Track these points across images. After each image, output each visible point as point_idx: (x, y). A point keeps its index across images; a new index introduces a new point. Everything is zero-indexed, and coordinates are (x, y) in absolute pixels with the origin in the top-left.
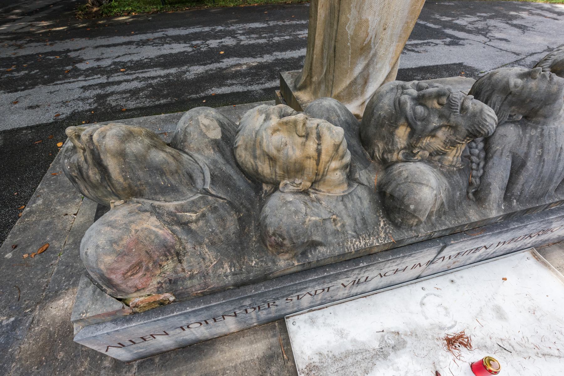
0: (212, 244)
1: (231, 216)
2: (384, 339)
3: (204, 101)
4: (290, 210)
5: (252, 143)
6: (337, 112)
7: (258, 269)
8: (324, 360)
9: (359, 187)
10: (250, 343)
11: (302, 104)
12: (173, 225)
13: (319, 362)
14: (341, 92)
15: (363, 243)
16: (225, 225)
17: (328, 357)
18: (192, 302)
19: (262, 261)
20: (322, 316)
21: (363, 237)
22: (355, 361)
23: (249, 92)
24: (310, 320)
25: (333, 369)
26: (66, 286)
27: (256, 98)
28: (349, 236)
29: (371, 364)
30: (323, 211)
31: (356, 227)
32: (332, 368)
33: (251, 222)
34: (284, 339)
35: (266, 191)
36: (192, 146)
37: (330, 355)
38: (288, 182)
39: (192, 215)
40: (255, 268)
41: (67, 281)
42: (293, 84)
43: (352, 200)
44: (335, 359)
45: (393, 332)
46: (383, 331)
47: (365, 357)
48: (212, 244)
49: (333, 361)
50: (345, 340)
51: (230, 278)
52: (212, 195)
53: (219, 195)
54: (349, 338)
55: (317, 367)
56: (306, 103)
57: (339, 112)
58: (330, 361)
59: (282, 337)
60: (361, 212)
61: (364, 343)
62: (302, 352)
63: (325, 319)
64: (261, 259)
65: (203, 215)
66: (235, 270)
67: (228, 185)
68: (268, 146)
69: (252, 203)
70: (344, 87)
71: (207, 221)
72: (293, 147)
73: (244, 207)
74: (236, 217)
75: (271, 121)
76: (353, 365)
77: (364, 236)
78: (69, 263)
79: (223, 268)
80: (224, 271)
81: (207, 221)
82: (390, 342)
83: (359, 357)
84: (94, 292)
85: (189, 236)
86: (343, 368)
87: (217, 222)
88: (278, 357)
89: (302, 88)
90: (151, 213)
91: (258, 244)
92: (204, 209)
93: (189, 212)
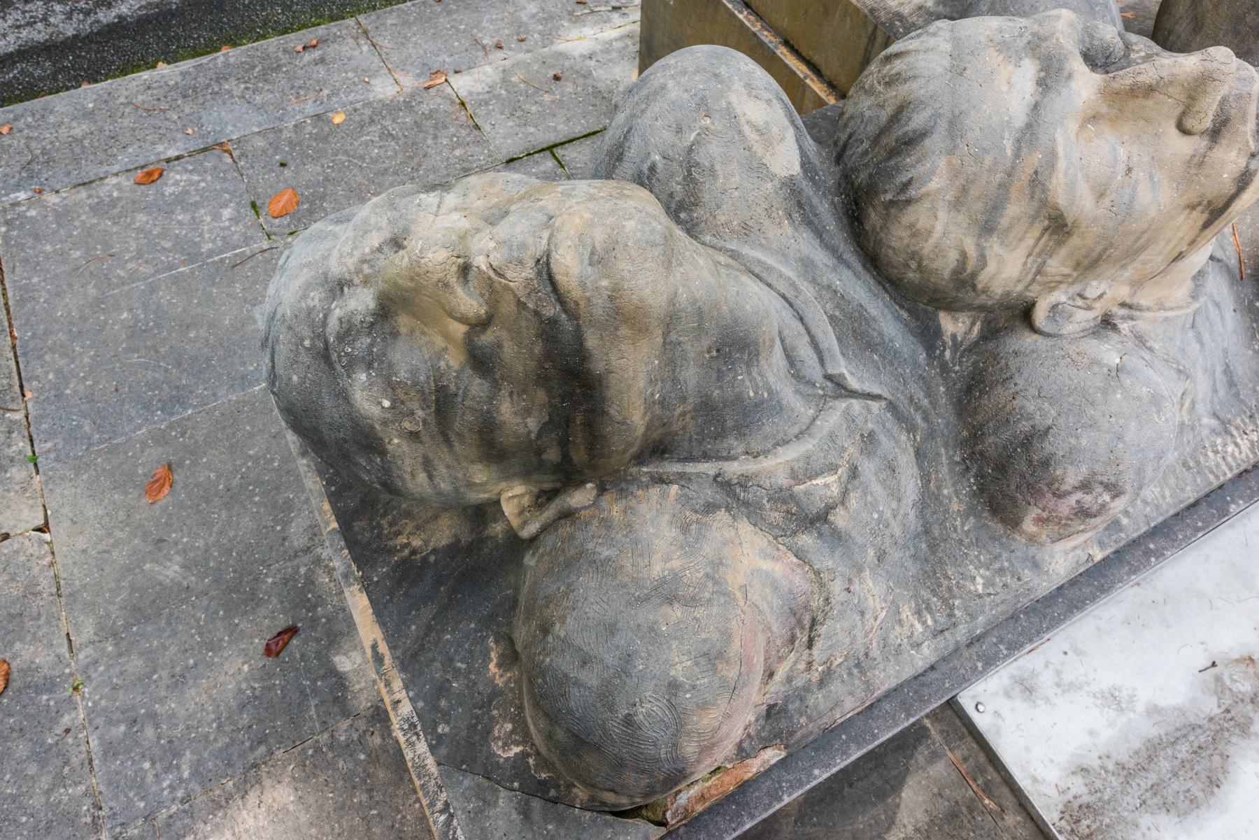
2: (1223, 685)
4: (1139, 399)
5: (999, 177)
7: (998, 599)
8: (1098, 784)
10: (878, 797)
12: (794, 533)
13: (1090, 793)
15: (1245, 445)
17: (1106, 771)
18: (816, 750)
19: (1001, 571)
20: (1046, 666)
21: (1237, 428)
22: (1177, 763)
24: (1018, 689)
25: (1130, 800)
26: (172, 788)
28: (1205, 432)
29: (1216, 758)
32: (1128, 799)
34: (965, 760)
35: (954, 337)
36: (722, 219)
37: (1111, 767)
38: (1063, 298)
40: (987, 600)
41: (167, 770)
44: (1127, 773)
45: (1237, 661)
46: (1214, 664)
47: (1196, 744)
49: (1121, 779)
50: (1131, 715)
51: (925, 649)
54: (1140, 708)
55: (1088, 807)
58: (1115, 782)
59: (958, 753)
61: (1180, 710)
62: (1035, 780)
64: (997, 565)
66: (935, 621)
68: (1071, 186)
72: (1151, 177)
75: (1074, 84)
76: (1176, 775)
77: (1238, 421)
78: (133, 708)
80: (906, 631)
82: (1243, 689)
83: (1183, 750)
84: (526, 814)
86: (1154, 789)
90: (728, 509)
91: (972, 519)
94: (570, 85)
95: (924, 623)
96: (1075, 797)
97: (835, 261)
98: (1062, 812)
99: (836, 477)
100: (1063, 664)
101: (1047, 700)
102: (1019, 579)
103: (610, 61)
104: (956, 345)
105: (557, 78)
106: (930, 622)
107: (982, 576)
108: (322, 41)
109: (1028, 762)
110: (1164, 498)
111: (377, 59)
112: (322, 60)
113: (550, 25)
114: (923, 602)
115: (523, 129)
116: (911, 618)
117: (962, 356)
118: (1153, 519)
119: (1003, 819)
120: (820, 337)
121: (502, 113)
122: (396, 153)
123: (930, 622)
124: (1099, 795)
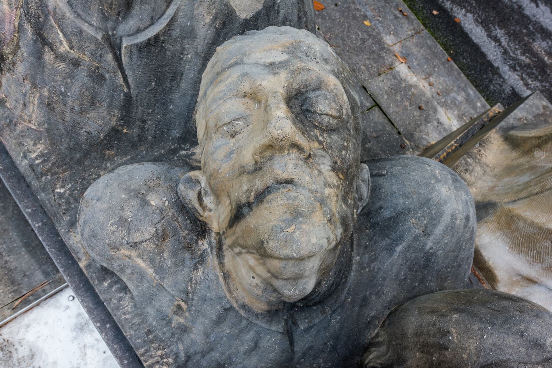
0: (49, 106)
1: (109, 113)
3: (435, 12)
4: (122, 209)
6: (435, 226)
9: (279, 336)
10: (26, 243)
11: (470, 156)
13: (18, 359)
14: (525, 220)
16: (87, 110)
20: (97, 340)
23: (496, 71)
27: (487, 87)
30: (180, 277)
31: (198, 357)
33: (126, 154)
35: (194, 154)
39: (65, 43)
40: (52, 196)
42: (516, 123)
43: (241, 331)
48: (49, 104)
51: (25, 162)
52: (118, 59)
53: (128, 72)
55: (10, 357)
56: (479, 162)
57: (439, 230)
60: (230, 358)
62: (28, 326)
63: (92, 347)
64: (72, 200)
65: (76, 63)
66: (38, 165)
67: (159, 80)
69: (159, 138)
70: (537, 221)
71: (71, 75)
73: (143, 129)
74: (113, 123)
79: (35, 144)
80: (32, 148)
81: (71, 75)
85: (31, 59)
87: (82, 94)
88: (14, 291)
89: (513, 142)
92: (86, 59)
93: (65, 35)
94: (418, 113)
95: (36, 158)
96: (16, 349)
97: (202, 55)
98: (8, 341)
99: (68, 49)
100: (98, 350)
101: (75, 338)
102: (64, 214)
103: (440, 132)
104: (189, 156)
105: (420, 108)
106: (37, 162)
107: (65, 192)
108: (407, 17)
109: (38, 323)
110: (125, 314)
111: (405, 37)
112: (396, 17)
113: (452, 106)
114: (48, 158)
115: (384, 93)
116: (39, 151)
117: (182, 160)
118: (109, 304)
119: (9, 309)
120: (144, 33)
121: (391, 85)
122: (355, 44)
123: (37, 162)
124: (17, 364)
